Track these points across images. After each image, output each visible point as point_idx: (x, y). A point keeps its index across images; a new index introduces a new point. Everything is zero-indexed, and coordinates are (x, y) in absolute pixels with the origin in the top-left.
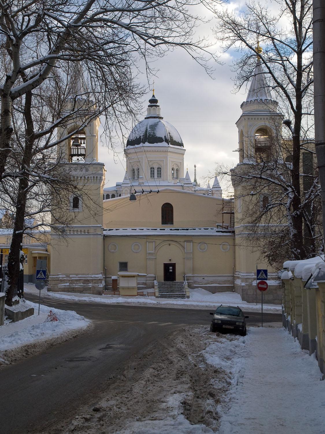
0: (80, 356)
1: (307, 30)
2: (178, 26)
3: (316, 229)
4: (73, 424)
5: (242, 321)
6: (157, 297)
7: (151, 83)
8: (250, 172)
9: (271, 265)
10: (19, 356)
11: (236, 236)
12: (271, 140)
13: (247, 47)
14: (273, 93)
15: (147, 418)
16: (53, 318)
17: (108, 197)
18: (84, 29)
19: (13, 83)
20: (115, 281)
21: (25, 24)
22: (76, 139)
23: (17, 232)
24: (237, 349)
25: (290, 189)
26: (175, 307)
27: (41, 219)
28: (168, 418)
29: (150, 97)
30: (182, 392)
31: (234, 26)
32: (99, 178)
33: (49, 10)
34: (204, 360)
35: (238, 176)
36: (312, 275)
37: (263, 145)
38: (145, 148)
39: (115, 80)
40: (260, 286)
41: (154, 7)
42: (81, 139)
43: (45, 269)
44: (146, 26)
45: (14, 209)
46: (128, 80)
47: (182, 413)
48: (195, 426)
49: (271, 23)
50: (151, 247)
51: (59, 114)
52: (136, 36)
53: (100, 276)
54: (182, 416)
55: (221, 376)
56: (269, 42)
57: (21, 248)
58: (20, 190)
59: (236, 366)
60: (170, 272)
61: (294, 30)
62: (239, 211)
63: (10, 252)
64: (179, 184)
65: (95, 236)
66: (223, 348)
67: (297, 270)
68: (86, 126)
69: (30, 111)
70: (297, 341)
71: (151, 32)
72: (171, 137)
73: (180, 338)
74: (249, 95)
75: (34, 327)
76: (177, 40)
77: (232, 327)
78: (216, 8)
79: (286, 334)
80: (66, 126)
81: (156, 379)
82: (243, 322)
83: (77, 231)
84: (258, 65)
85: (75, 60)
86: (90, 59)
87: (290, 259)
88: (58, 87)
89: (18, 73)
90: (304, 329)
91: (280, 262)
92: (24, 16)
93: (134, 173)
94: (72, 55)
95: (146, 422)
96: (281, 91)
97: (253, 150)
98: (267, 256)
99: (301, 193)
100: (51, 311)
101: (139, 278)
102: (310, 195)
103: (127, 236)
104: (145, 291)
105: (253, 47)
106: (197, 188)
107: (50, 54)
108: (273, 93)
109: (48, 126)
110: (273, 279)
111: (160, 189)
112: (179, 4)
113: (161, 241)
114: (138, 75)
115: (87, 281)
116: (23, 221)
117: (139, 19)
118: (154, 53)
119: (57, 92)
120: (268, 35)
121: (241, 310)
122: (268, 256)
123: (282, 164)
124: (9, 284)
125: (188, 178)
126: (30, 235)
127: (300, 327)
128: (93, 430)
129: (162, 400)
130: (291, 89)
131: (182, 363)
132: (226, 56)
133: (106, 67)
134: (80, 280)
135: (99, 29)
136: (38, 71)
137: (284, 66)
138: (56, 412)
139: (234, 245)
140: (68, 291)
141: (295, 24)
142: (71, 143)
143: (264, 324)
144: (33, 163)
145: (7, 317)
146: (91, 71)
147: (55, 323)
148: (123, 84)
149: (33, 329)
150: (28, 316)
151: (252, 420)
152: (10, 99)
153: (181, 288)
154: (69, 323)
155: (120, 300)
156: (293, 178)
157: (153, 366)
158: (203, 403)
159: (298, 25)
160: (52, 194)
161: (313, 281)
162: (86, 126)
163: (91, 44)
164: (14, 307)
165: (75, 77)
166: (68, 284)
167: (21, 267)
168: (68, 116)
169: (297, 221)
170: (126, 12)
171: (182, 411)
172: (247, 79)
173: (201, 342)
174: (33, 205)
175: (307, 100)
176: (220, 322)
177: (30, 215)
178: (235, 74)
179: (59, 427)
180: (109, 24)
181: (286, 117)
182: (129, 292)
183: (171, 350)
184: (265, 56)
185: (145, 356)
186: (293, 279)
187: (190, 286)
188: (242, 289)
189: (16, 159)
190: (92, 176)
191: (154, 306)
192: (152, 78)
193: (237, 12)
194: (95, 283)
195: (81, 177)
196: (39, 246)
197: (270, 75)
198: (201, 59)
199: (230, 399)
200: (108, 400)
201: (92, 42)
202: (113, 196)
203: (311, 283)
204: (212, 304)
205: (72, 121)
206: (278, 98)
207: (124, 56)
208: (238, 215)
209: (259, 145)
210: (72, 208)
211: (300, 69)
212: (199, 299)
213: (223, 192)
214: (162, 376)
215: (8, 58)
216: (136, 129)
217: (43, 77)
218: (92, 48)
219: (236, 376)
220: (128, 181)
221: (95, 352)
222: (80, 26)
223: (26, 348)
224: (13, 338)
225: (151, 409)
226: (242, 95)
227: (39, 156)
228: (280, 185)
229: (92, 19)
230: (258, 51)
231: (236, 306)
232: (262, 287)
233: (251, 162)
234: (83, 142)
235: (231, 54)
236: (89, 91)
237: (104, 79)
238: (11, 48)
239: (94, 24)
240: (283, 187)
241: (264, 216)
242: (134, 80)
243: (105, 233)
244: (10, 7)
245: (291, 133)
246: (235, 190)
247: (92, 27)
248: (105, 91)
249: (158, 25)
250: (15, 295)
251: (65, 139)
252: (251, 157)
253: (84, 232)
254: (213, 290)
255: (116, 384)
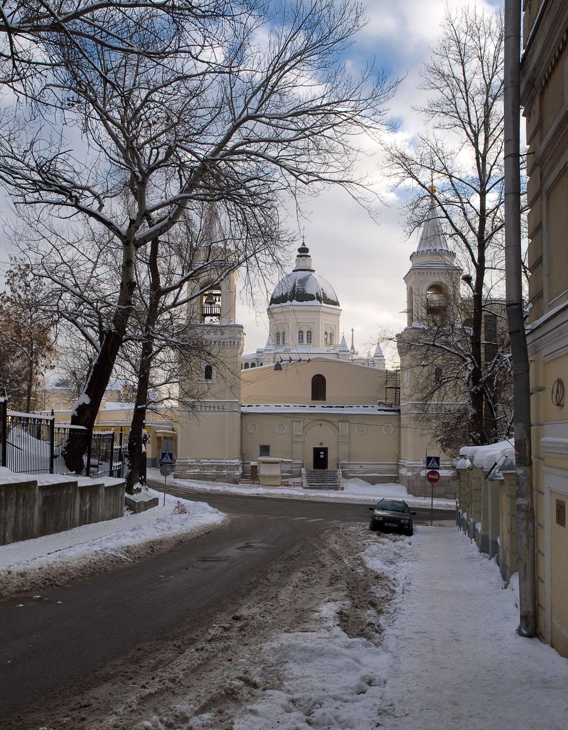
0: (214, 556)
1: (492, 167)
2: (337, 160)
3: (500, 408)
4: (210, 634)
5: (408, 518)
6: (305, 488)
7: (302, 228)
8: (421, 338)
9: (445, 451)
10: (143, 553)
11: (402, 416)
12: (447, 300)
13: (419, 186)
14: (450, 243)
15: (296, 629)
16: (182, 510)
17: (247, 366)
18: (223, 162)
19: (138, 228)
20: (254, 468)
21: (153, 158)
22: (211, 296)
23: (139, 407)
24: (402, 551)
25: (469, 359)
26: (327, 500)
27: (167, 392)
28: (322, 630)
29: (300, 246)
30: (337, 601)
31: (403, 160)
32: (236, 343)
33: (181, 141)
34: (362, 564)
35: (405, 343)
36: (496, 464)
37: (438, 305)
38: (294, 307)
39: (258, 224)
40: (430, 476)
41: (307, 136)
42: (216, 295)
43: (171, 452)
44: (297, 159)
45: (135, 379)
46: (275, 225)
47: (338, 625)
48: (353, 640)
49: (449, 157)
50: (298, 429)
51: (190, 265)
52: (285, 172)
53: (237, 462)
54: (339, 628)
55: (384, 582)
56: (446, 180)
57: (143, 426)
58: (142, 356)
59: (401, 572)
60: (320, 459)
61: (476, 167)
62: (407, 386)
63: (130, 430)
64: (332, 352)
65: (232, 414)
66: (386, 549)
67: (477, 458)
68: (222, 280)
69: (155, 262)
70: (474, 543)
71: (303, 166)
72: (324, 294)
73: (333, 537)
74: (420, 243)
75: (159, 521)
76: (335, 177)
77: (395, 526)
78: (382, 138)
79: (461, 534)
80: (198, 280)
81: (305, 584)
82: (409, 520)
83: (210, 407)
84: (432, 208)
85: (211, 200)
86: (229, 200)
87: (467, 444)
88: (189, 232)
89: (143, 217)
90: (485, 528)
91: (456, 448)
92: (153, 149)
93: (278, 337)
94: (208, 195)
95: (296, 633)
96: (460, 239)
97: (425, 311)
98: (440, 440)
99: (483, 365)
100: (179, 502)
101: (283, 465)
102: (494, 367)
103: (269, 414)
104: (291, 481)
105: (427, 186)
106: (355, 357)
107: (181, 193)
108: (450, 243)
109: (176, 279)
110: (446, 468)
111: (311, 357)
112: (338, 134)
113: (310, 421)
114: (286, 218)
115: (221, 467)
116: (146, 393)
117: (289, 151)
118: (307, 192)
119: (188, 239)
120: (444, 171)
121: (407, 506)
122: (441, 441)
123: (459, 329)
124: (129, 468)
125: (344, 344)
126: (155, 411)
127: (479, 526)
128: (233, 641)
129: (314, 609)
130: (472, 237)
131: (337, 567)
132: (392, 197)
133: (248, 209)
134: (213, 465)
135: (241, 164)
136: (166, 214)
137: (464, 209)
138: (189, 619)
139: (399, 427)
140: (199, 479)
141: (477, 159)
142: (204, 301)
143: (434, 522)
144: (158, 323)
145: (127, 507)
146: (230, 213)
147: (184, 516)
148: (267, 229)
149: (158, 522)
150: (151, 507)
151: (422, 634)
152: (133, 247)
153: (334, 478)
154: (201, 517)
155: (261, 491)
156: (473, 346)
157: (302, 570)
158: (363, 613)
159: (481, 161)
160: (180, 362)
161: (497, 471)
162: (222, 280)
163: (231, 182)
164: (135, 495)
165: (210, 221)
166: (198, 470)
167: (144, 449)
168: (201, 268)
169: (477, 398)
170: (273, 143)
171: (338, 623)
172: (419, 224)
173: (359, 543)
174: (158, 375)
175: (491, 251)
176: (381, 519)
177: (154, 387)
178: (404, 219)
179: (193, 636)
180: (253, 157)
181: (466, 272)
182: (271, 481)
183: (323, 551)
184: (441, 197)
185: (291, 558)
186: (471, 469)
187: (345, 476)
188: (408, 481)
189: (139, 319)
190: (228, 341)
191: (300, 499)
192: (303, 223)
193: (407, 144)
194: (230, 470)
195: (215, 342)
196: (164, 424)
197: (446, 220)
198: (364, 199)
199: (395, 610)
200: (249, 608)
201: (232, 179)
202: (253, 365)
203: (495, 473)
204: (371, 498)
205: (206, 273)
206: (457, 248)
207: (270, 196)
208: (405, 391)
209: (432, 305)
210: (204, 379)
211: (483, 214)
212: (355, 491)
213: (386, 362)
214: (313, 582)
215: (132, 198)
216: (283, 284)
217: (172, 221)
218: (232, 186)
219: (402, 583)
220: (271, 347)
221: (232, 552)
222: (218, 160)
223: (151, 544)
224: (135, 532)
225: (301, 618)
226: (413, 244)
227: (166, 316)
228: (457, 354)
229: (233, 152)
230: (432, 191)
231: (401, 500)
232: (433, 478)
233: (422, 326)
234: (217, 299)
235: (399, 194)
236: (227, 237)
237: (245, 222)
238: (136, 187)
239: (236, 157)
240: (461, 357)
241: (436, 392)
242: (282, 224)
243: (243, 409)
244: (137, 138)
245: (471, 291)
246: (402, 360)
247: (232, 161)
248: (247, 238)
249: (312, 158)
250: (136, 482)
251: (197, 296)
252: (422, 319)
253: (218, 408)
254: (373, 481)
255: (258, 589)
